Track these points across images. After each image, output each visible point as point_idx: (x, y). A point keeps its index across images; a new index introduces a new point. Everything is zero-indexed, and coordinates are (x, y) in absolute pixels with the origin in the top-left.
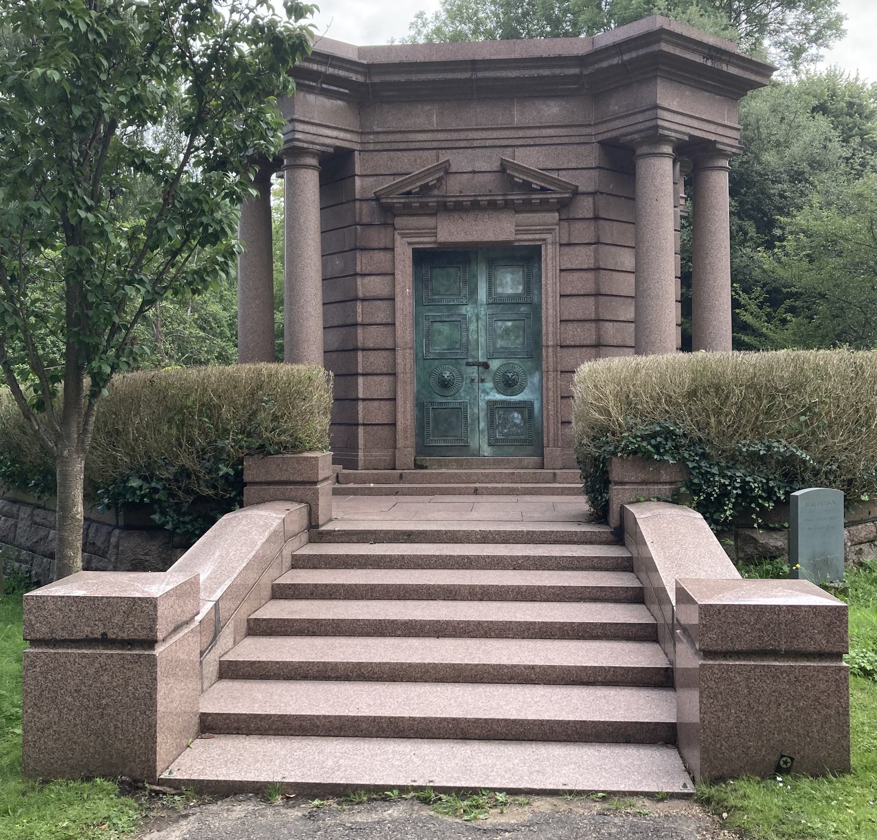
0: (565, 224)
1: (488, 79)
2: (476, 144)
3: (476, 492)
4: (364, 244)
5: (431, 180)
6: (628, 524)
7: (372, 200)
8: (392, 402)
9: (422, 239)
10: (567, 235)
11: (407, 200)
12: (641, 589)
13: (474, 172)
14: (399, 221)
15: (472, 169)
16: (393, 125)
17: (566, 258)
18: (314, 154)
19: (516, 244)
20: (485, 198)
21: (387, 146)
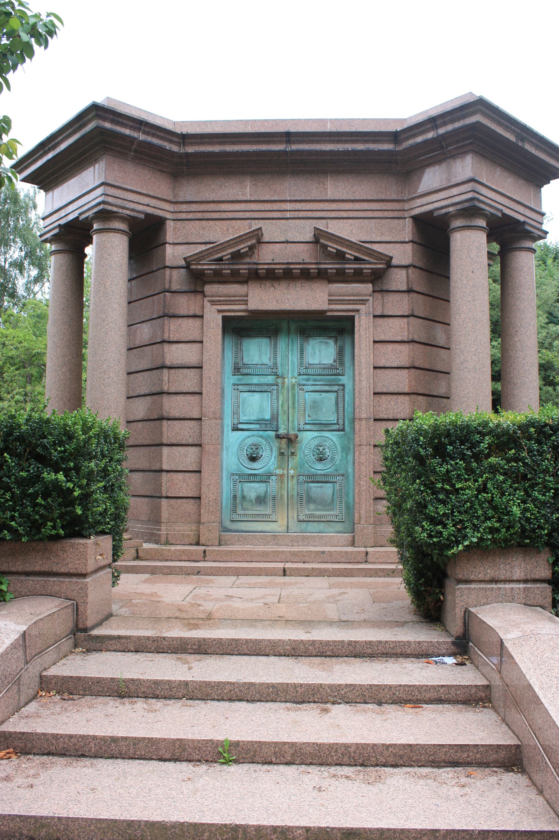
0: (378, 296)
1: (302, 152)
2: (288, 215)
3: (285, 572)
4: (172, 311)
5: (243, 247)
6: (474, 631)
7: (182, 267)
8: (198, 474)
9: (232, 307)
10: (380, 307)
11: (218, 267)
12: (518, 746)
13: (287, 242)
14: (209, 289)
15: (287, 238)
16: (207, 195)
17: (379, 330)
18: (123, 219)
19: (329, 314)
20: (298, 266)
21: (199, 216)
